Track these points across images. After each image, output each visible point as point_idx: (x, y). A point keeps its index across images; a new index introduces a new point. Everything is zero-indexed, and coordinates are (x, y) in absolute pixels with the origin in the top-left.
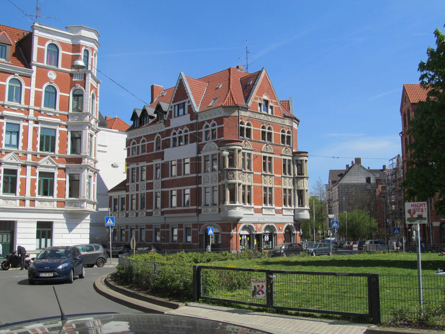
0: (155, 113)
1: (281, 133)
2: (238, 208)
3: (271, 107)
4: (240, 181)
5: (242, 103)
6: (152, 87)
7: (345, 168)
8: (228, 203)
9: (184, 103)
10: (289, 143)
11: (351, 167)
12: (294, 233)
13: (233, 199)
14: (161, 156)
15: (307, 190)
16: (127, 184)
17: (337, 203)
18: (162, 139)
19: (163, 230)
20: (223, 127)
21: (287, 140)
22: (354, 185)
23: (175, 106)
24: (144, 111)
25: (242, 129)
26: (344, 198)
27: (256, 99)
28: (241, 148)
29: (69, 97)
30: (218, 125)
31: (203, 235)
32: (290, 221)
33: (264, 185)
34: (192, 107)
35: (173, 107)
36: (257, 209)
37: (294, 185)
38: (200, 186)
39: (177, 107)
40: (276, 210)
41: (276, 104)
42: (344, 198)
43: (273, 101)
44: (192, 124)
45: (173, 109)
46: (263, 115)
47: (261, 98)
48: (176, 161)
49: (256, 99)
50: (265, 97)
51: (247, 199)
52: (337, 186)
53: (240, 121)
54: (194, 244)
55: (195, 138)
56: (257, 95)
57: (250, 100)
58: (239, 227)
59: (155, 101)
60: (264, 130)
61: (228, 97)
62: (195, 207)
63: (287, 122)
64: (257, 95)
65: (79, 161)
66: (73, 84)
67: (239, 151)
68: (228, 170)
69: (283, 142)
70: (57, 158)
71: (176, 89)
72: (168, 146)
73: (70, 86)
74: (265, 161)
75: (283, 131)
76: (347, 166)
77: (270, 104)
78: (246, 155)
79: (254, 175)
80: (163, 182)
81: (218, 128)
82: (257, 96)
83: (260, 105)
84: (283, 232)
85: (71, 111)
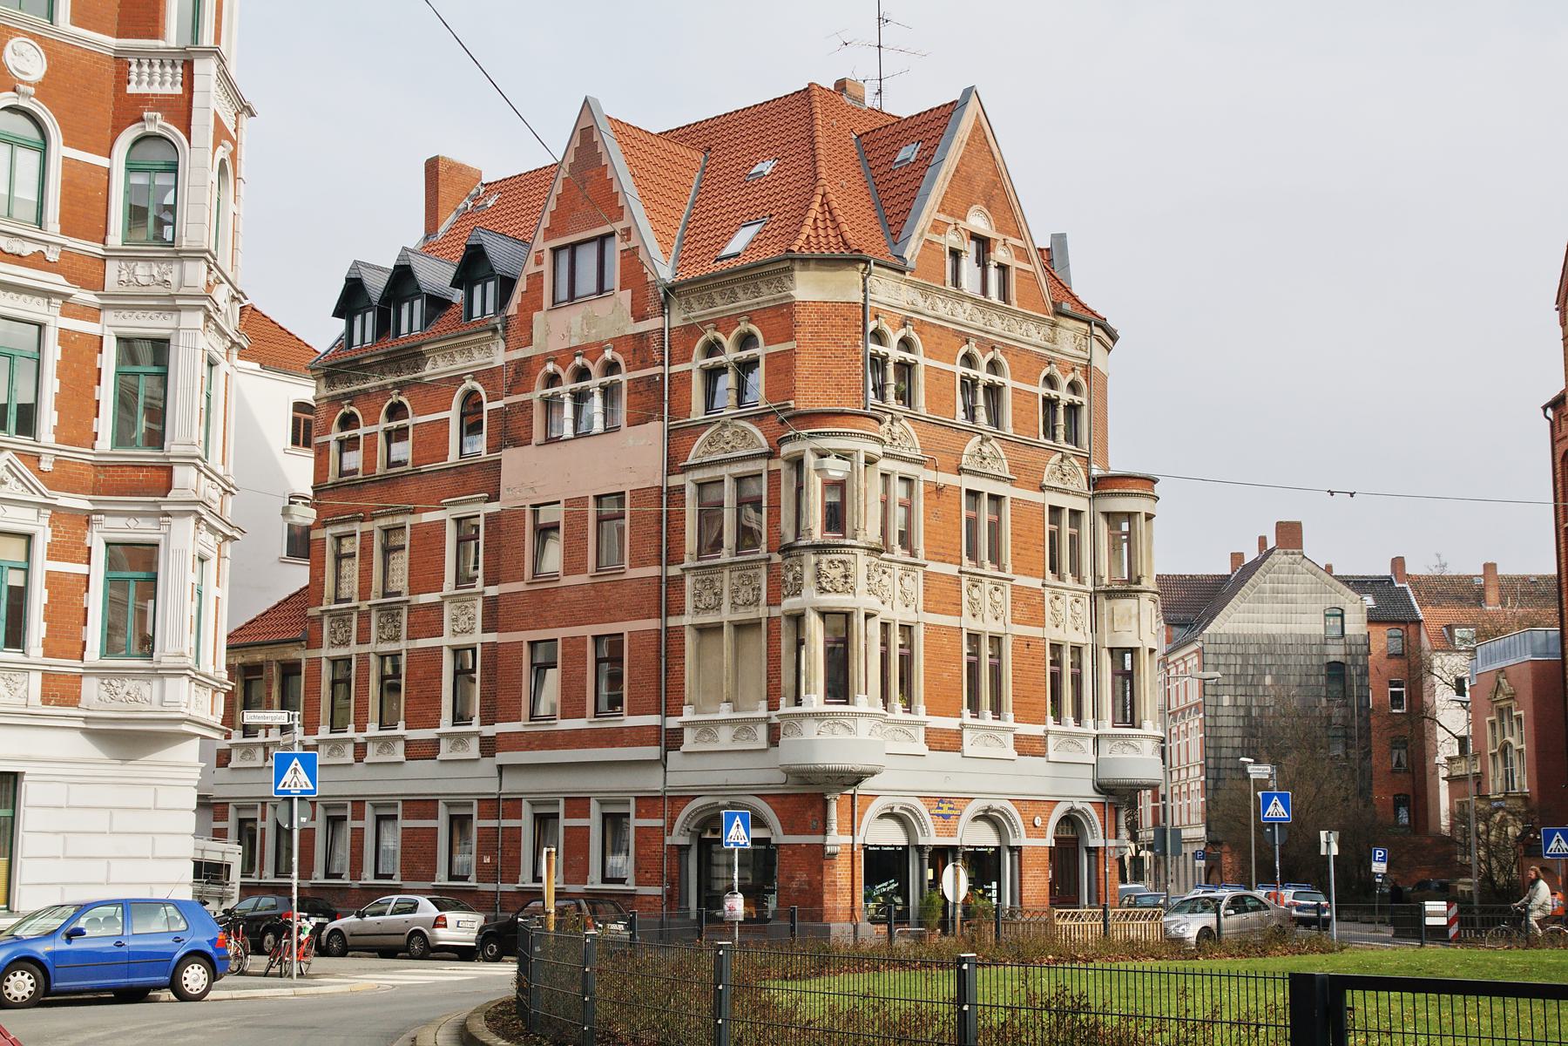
0: (456, 283)
1: (1042, 390)
2: (863, 723)
3: (1003, 268)
4: (872, 603)
5: (875, 245)
6: (432, 167)
7: (1225, 568)
8: (815, 700)
9: (602, 240)
10: (1073, 436)
11: (1256, 564)
12: (1092, 844)
13: (839, 688)
14: (486, 478)
15: (1152, 651)
16: (313, 612)
17: (1195, 722)
18: (487, 407)
19: (493, 823)
20: (791, 353)
21: (1065, 418)
22: (1270, 645)
23: (555, 251)
24: (402, 276)
25: (878, 363)
26: (1226, 701)
27: (938, 227)
28: (877, 449)
29: (108, 172)
30: (768, 343)
31: (688, 847)
32: (1080, 793)
33: (969, 623)
34: (642, 256)
35: (547, 257)
36: (942, 731)
37: (1094, 628)
38: (673, 622)
39: (564, 258)
40: (929, 732)
41: (1022, 254)
42: (1226, 701)
43: (1012, 240)
44: (641, 337)
45: (546, 267)
46: (968, 305)
47: (962, 224)
48: (561, 508)
49: (938, 227)
50: (978, 222)
51: (900, 681)
52: (1194, 647)
53: (871, 326)
54: (643, 890)
55: (651, 400)
56: (942, 210)
57: (915, 235)
58: (862, 814)
59: (442, 229)
60: (972, 373)
61: (812, 214)
62: (653, 720)
63: (1069, 337)
64: (942, 210)
65: (162, 479)
66: (129, 110)
67: (870, 461)
68: (820, 548)
69: (1050, 431)
70: (46, 465)
71: (564, 174)
72: (521, 441)
73: (115, 118)
74: (973, 514)
75: (1050, 381)
76: (1237, 557)
77: (999, 254)
78: (894, 481)
79: (926, 575)
80: (491, 605)
81: (634, 383)
82: (942, 217)
83: (956, 254)
84: (1049, 841)
85: (115, 238)
